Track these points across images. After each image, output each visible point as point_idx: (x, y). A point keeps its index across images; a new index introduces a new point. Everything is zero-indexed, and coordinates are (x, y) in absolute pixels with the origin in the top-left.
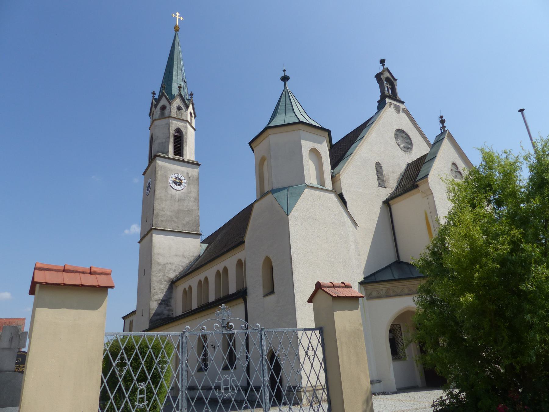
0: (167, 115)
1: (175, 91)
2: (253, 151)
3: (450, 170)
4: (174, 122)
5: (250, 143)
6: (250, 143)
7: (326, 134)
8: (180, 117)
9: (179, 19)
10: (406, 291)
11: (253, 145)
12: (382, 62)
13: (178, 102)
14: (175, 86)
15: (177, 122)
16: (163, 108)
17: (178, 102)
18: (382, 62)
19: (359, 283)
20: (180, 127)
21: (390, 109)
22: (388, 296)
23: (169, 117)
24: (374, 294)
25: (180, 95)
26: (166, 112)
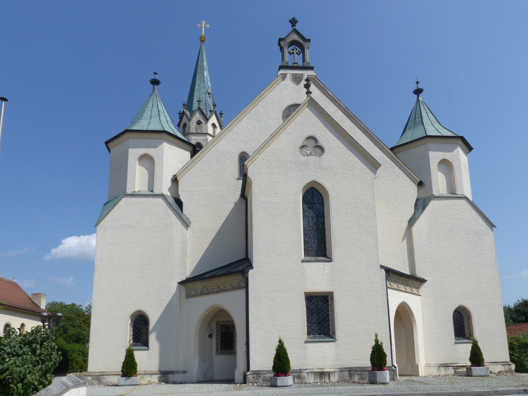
0: (187, 132)
1: (195, 106)
2: (109, 151)
3: (298, 147)
4: (193, 137)
5: (107, 143)
6: (107, 143)
7: (460, 141)
8: (199, 131)
9: (205, 27)
10: (216, 289)
11: (110, 145)
12: (293, 22)
13: (197, 116)
14: (195, 100)
15: (196, 137)
16: (185, 125)
17: (197, 116)
18: (293, 22)
19: (179, 283)
20: (200, 141)
21: (284, 82)
22: (202, 294)
23: (189, 133)
24: (193, 292)
25: (200, 109)
26: (187, 129)
